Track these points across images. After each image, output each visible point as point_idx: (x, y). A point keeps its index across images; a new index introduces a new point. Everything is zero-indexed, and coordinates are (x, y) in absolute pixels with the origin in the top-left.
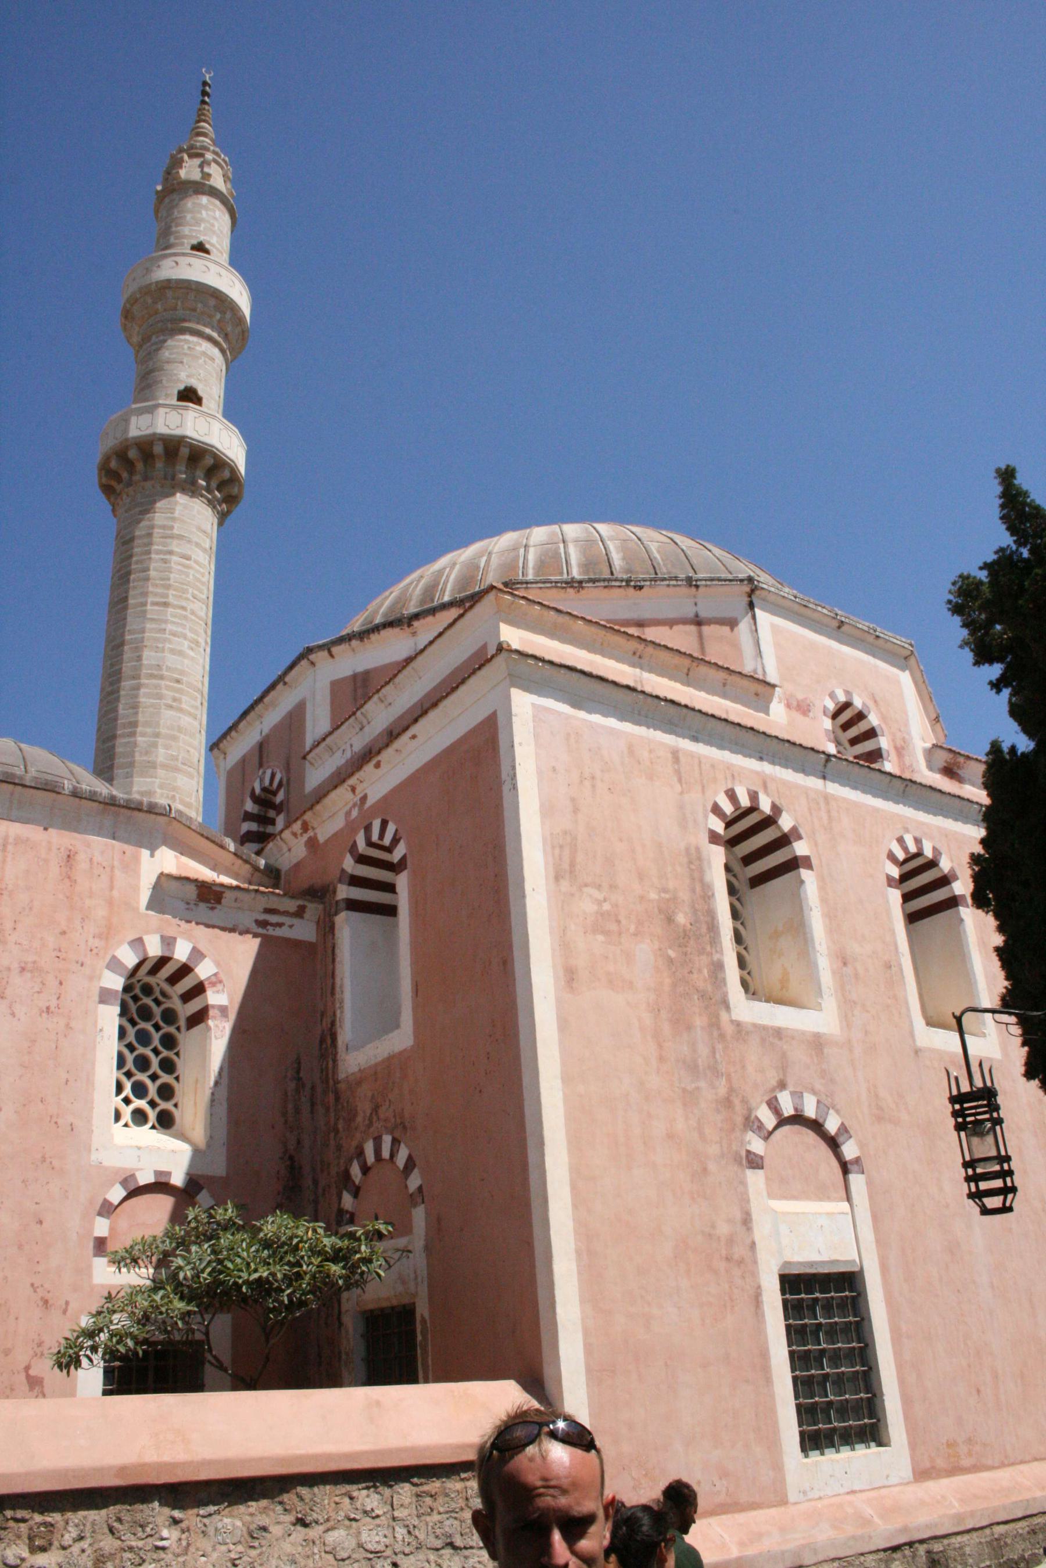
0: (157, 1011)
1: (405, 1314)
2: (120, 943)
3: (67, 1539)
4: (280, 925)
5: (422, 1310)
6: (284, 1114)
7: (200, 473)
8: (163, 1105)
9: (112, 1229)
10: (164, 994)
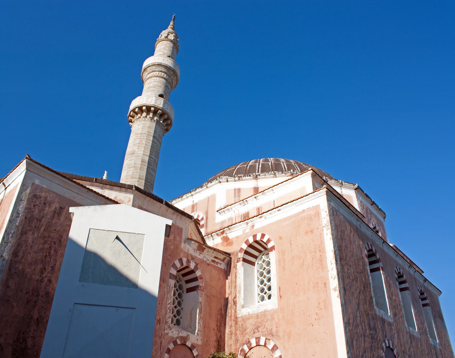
6: (217, 326)
8: (178, 317)
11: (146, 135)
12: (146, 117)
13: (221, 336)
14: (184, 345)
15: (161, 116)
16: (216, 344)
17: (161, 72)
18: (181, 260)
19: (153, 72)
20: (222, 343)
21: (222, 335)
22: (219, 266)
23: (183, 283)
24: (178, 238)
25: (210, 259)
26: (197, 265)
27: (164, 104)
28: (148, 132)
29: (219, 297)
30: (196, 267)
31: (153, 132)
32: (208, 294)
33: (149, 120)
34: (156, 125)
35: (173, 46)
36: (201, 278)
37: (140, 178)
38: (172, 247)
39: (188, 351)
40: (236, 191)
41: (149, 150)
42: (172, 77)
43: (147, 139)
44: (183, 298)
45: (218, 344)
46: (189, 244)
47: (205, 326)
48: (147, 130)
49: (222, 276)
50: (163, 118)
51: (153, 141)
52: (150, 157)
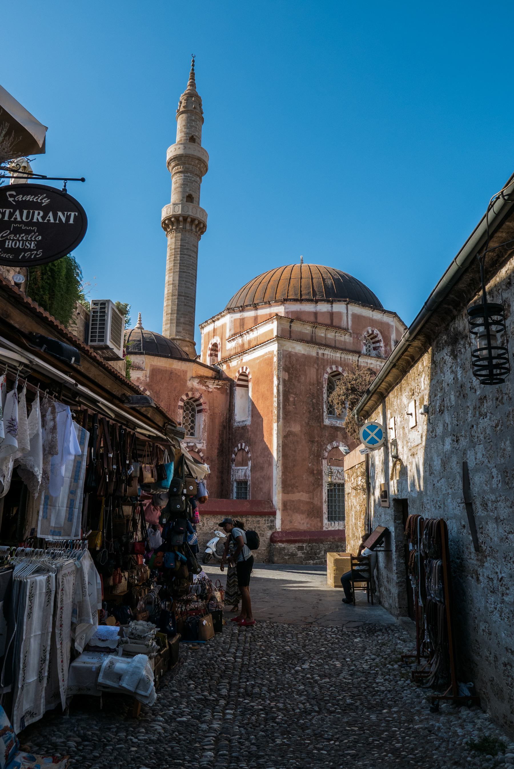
7: (194, 226)
18: (187, 395)
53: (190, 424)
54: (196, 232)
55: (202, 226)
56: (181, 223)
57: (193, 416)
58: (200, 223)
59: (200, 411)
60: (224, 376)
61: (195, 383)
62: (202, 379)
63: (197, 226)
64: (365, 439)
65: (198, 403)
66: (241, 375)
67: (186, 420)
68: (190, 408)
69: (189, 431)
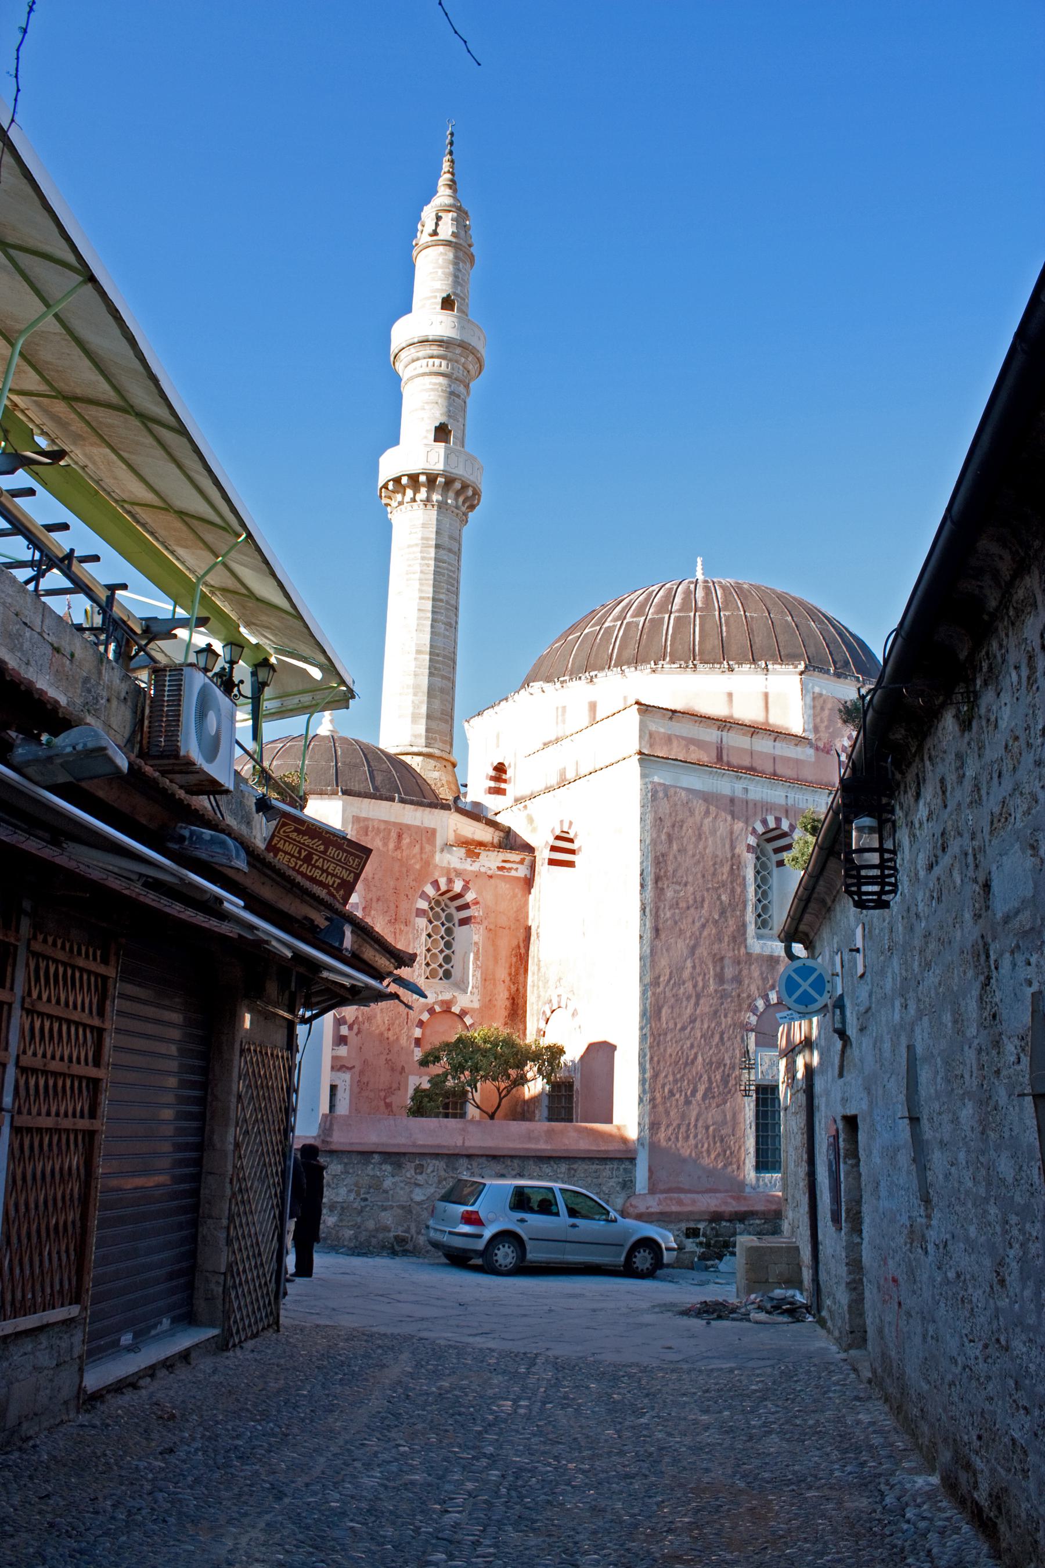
0: (443, 915)
1: (569, 1085)
2: (426, 883)
3: (429, 1171)
4: (510, 869)
5: (577, 1085)
6: (510, 974)
7: (451, 494)
8: (446, 967)
9: (423, 1034)
10: (446, 905)
11: (419, 549)
12: (414, 500)
13: (517, 990)
14: (447, 1011)
15: (449, 483)
16: (508, 1003)
17: (432, 357)
18: (436, 884)
19: (413, 361)
20: (520, 1002)
21: (521, 987)
22: (513, 873)
23: (453, 911)
24: (428, 848)
25: (494, 867)
26: (467, 883)
27: (447, 457)
28: (423, 539)
29: (513, 927)
30: (466, 888)
31: (433, 536)
32: (492, 927)
33: (422, 506)
34: (438, 515)
35: (456, 257)
36: (477, 903)
37: (418, 652)
38: (418, 867)
39: (457, 1019)
40: (560, 710)
41: (431, 582)
42: (463, 360)
43: (423, 558)
44: (455, 935)
45: (513, 1004)
46: (449, 852)
47: (487, 979)
48: (420, 535)
49: (519, 892)
50: (453, 493)
51: (436, 559)
52: (434, 599)
53: (441, 951)
54: (457, 507)
55: (470, 493)
56: (423, 490)
57: (449, 932)
58: (465, 487)
59: (464, 922)
60: (519, 841)
61: (455, 859)
62: (472, 848)
63: (458, 494)
64: (795, 971)
65: (459, 902)
66: (558, 838)
67: (435, 928)
68: (443, 915)
69: (441, 966)
